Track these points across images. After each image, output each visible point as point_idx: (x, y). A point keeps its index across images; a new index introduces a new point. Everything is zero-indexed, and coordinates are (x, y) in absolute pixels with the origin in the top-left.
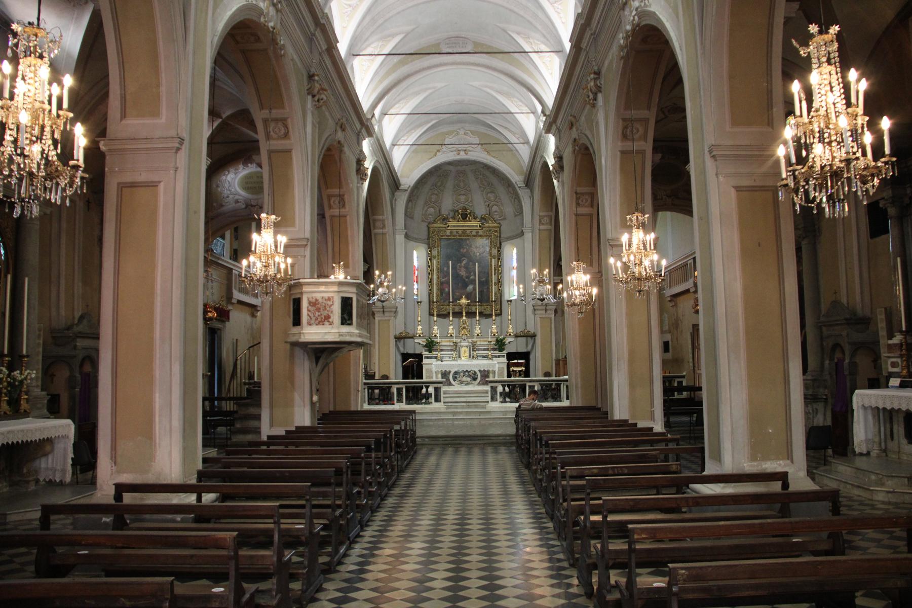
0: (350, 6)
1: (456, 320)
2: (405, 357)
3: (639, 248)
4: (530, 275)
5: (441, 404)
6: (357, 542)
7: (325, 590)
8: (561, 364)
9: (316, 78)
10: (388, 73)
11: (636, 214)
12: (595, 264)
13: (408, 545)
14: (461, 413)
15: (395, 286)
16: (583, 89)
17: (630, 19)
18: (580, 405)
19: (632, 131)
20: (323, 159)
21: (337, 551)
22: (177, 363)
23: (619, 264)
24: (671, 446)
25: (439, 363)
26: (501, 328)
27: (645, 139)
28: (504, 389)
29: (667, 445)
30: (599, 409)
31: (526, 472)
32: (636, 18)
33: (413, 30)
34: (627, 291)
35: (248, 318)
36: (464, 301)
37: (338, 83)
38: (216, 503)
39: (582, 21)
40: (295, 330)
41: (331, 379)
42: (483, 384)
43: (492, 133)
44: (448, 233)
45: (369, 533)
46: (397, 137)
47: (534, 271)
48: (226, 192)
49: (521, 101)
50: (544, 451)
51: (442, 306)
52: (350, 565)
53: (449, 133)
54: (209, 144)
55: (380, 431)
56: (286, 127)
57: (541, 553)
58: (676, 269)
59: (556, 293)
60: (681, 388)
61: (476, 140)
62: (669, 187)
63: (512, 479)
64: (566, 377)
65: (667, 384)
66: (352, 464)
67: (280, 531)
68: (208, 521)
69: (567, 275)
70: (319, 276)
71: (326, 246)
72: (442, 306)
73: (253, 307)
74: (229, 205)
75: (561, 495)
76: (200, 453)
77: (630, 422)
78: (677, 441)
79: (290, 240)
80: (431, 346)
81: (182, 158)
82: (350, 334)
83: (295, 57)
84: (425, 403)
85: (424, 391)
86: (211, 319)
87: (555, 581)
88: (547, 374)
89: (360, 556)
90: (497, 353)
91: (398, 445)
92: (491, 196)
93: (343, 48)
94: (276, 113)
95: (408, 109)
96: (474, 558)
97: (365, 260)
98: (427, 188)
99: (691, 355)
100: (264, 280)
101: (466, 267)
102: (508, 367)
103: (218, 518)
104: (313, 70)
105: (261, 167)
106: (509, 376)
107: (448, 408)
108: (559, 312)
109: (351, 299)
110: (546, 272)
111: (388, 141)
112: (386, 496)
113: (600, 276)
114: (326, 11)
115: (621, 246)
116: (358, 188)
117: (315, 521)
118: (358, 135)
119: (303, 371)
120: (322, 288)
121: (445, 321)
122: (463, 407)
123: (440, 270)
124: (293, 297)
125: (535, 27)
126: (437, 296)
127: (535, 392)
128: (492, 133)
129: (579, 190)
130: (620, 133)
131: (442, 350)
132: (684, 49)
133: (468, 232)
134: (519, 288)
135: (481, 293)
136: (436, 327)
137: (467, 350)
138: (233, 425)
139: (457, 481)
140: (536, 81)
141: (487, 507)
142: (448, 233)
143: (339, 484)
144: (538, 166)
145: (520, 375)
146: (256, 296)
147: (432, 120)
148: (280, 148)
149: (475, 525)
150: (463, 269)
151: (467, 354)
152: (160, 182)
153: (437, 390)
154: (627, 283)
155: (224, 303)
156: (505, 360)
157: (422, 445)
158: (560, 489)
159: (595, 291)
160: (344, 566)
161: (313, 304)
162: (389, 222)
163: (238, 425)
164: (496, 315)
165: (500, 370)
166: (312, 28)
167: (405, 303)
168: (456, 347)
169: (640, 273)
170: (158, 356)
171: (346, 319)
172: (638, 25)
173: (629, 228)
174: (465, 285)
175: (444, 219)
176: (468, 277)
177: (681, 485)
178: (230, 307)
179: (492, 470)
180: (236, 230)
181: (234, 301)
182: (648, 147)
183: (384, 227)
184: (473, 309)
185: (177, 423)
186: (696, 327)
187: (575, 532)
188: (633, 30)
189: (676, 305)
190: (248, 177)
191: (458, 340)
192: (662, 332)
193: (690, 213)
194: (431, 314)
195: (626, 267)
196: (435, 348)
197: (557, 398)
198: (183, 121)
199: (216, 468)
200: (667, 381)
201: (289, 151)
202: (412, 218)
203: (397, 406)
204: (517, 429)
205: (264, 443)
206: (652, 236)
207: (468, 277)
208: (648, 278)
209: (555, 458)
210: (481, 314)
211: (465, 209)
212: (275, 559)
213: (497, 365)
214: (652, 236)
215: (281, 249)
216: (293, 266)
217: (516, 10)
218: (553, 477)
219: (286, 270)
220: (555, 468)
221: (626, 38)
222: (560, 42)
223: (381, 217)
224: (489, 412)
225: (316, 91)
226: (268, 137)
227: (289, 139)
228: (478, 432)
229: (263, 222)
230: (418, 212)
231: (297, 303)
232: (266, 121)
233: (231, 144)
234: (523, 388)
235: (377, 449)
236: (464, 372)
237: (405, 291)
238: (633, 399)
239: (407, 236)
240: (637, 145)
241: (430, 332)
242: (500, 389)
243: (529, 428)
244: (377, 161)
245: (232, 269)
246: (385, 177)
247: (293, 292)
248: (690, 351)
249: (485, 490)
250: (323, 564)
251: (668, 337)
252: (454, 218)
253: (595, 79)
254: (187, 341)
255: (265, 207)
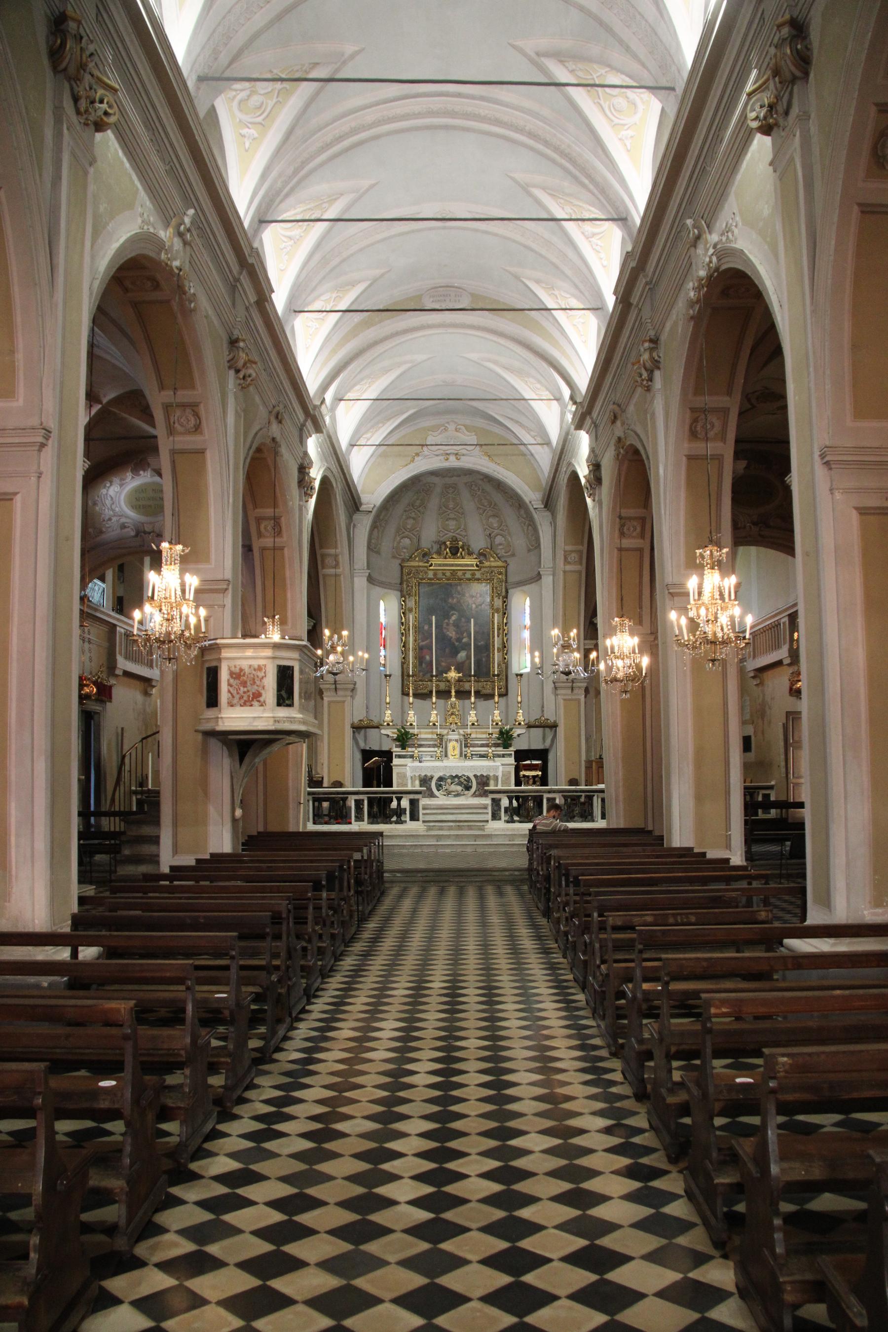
0: (290, 238)
1: (441, 702)
2: (367, 755)
3: (714, 598)
4: (550, 637)
5: (420, 823)
6: (302, 1020)
7: (257, 1087)
8: (595, 768)
9: (242, 344)
10: (345, 339)
11: (710, 547)
12: (646, 619)
13: (375, 1025)
14: (448, 837)
15: (353, 653)
16: (633, 364)
17: (703, 261)
18: (622, 826)
19: (704, 427)
20: (250, 465)
21: (273, 1032)
22: (43, 758)
23: (684, 621)
24: (755, 884)
25: (417, 764)
26: (506, 714)
27: (723, 439)
28: (511, 803)
29: (750, 884)
30: (650, 832)
31: (543, 921)
32: (714, 259)
33: (382, 275)
34: (694, 661)
35: (139, 697)
36: (453, 675)
37: (273, 353)
38: (100, 961)
39: (633, 264)
40: (211, 713)
41: (261, 787)
42: (480, 796)
43: (497, 430)
44: (431, 575)
45: (319, 1007)
46: (357, 435)
47: (555, 632)
48: (108, 513)
49: (539, 382)
50: (571, 892)
51: (420, 682)
52: (291, 1054)
53: (434, 428)
54: (88, 439)
55: (332, 861)
56: (197, 415)
57: (569, 1037)
58: (764, 631)
59: (586, 663)
60: (767, 805)
61: (472, 439)
62: (758, 508)
63: (524, 932)
64: (601, 786)
65: (748, 798)
66: (295, 908)
67: (196, 1002)
68: (86, 987)
69: (605, 637)
70: (244, 636)
71: (254, 589)
72: (420, 682)
73: (147, 682)
74: (112, 532)
75: (598, 955)
76: (75, 890)
77: (696, 851)
78: (766, 878)
79: (203, 581)
80: (404, 739)
81: (48, 456)
82: (291, 720)
83: (211, 312)
84: (396, 822)
85: (394, 804)
86: (88, 696)
87: (589, 1077)
88: (573, 782)
89: (307, 1039)
90: (500, 750)
91: (359, 883)
92: (494, 522)
93: (279, 300)
94: (184, 396)
95: (373, 391)
96: (472, 1043)
97: (310, 615)
98: (400, 509)
99: (783, 757)
100: (165, 640)
101: (456, 625)
102: (517, 769)
103: (103, 982)
104: (236, 333)
105: (160, 475)
106: (518, 783)
107: (430, 829)
108: (592, 691)
109: (291, 669)
110: (573, 633)
111: (344, 439)
112: (342, 954)
113: (653, 641)
114: (256, 245)
115: (688, 594)
116: (301, 509)
117: (244, 989)
118: (301, 430)
119: (222, 771)
120: (249, 653)
121: (425, 704)
122: (450, 828)
123: (418, 629)
124: (207, 665)
125: (563, 272)
126: (414, 667)
127: (556, 807)
128: (497, 430)
129: (625, 513)
130: (687, 427)
131: (420, 746)
132: (786, 307)
133: (460, 574)
134: (533, 657)
135: (478, 663)
136: (411, 713)
137: (457, 745)
138: (119, 852)
139: (445, 933)
140: (563, 353)
141: (488, 970)
142: (431, 575)
143: (277, 937)
144: (563, 480)
145: (534, 783)
146: (150, 665)
147: (408, 410)
148: (190, 447)
149: (472, 996)
150: (452, 628)
151: (457, 752)
152: (16, 494)
153: (414, 803)
154: (694, 648)
155: (104, 675)
156: (511, 760)
157: (392, 882)
158: (597, 945)
159: (645, 661)
160: (283, 1054)
161: (237, 675)
162: (344, 559)
163: (127, 852)
164: (500, 695)
165: (506, 776)
166: (235, 268)
167: (368, 678)
168: (441, 742)
169: (715, 634)
170: (13, 747)
171: (284, 697)
172: (717, 269)
173: (699, 568)
174: (455, 652)
175: (425, 555)
176: (459, 640)
177: (773, 940)
178: (113, 681)
179: (495, 919)
180: (121, 568)
181: (118, 672)
182: (728, 450)
183: (337, 566)
184: (467, 686)
185: (41, 845)
186: (793, 717)
187: (618, 1008)
188: (710, 277)
189: (761, 684)
190: (140, 490)
191: (445, 732)
192: (744, 723)
193: (789, 548)
194: (405, 694)
195: (693, 625)
196: (410, 742)
197: (587, 815)
198: (50, 404)
199: (98, 912)
200: (749, 792)
201: (202, 452)
202: (378, 553)
203: (355, 827)
204: (531, 863)
205: (164, 877)
206: (732, 580)
207: (459, 640)
208: (725, 642)
209: (588, 902)
210: (478, 694)
211: (455, 540)
212: (188, 1040)
213: (500, 768)
214: (732, 580)
215: (190, 595)
216: (207, 620)
217: (534, 246)
218: (586, 928)
219: (198, 627)
220: (589, 916)
221: (698, 289)
222: (598, 294)
223: (332, 551)
224: (489, 836)
225: (240, 364)
226: (171, 431)
227: (201, 433)
228: (473, 864)
229: (164, 554)
230: (386, 545)
231: (213, 674)
232: (167, 408)
233: (116, 442)
234: (538, 801)
235: (330, 889)
236: (453, 777)
237: (368, 661)
238: (700, 819)
239: (370, 580)
240: (713, 447)
241: (404, 719)
242: (505, 802)
243: (549, 858)
244: (328, 469)
245: (115, 626)
246: (338, 493)
247: (207, 658)
248: (782, 750)
249: (485, 948)
250: (253, 1050)
251: (750, 731)
252: (439, 553)
253: (651, 350)
254: (55, 725)
255: (167, 534)
